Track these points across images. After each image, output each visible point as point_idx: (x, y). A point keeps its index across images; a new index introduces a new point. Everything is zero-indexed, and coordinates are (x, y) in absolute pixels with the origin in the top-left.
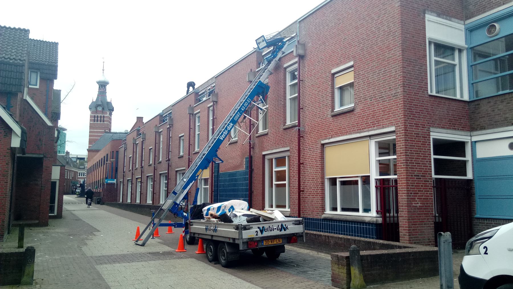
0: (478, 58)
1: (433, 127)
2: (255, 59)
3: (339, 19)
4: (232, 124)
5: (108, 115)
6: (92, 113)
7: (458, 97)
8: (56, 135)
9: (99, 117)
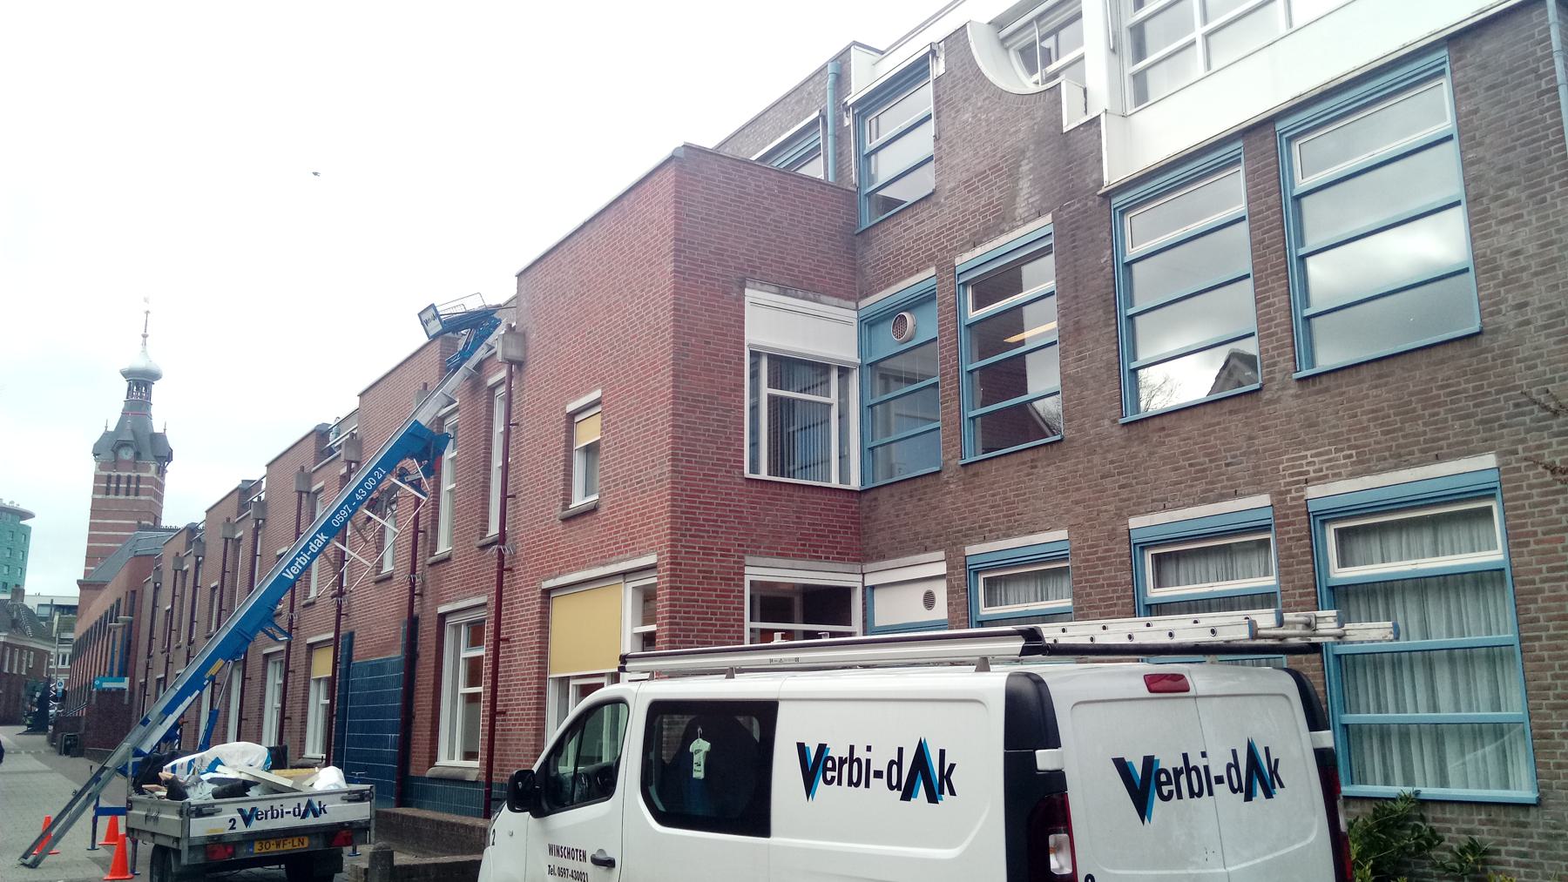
0: (893, 383)
1: (753, 554)
2: (437, 357)
3: (582, 284)
4: (323, 538)
5: (152, 473)
6: (102, 467)
7: (835, 482)
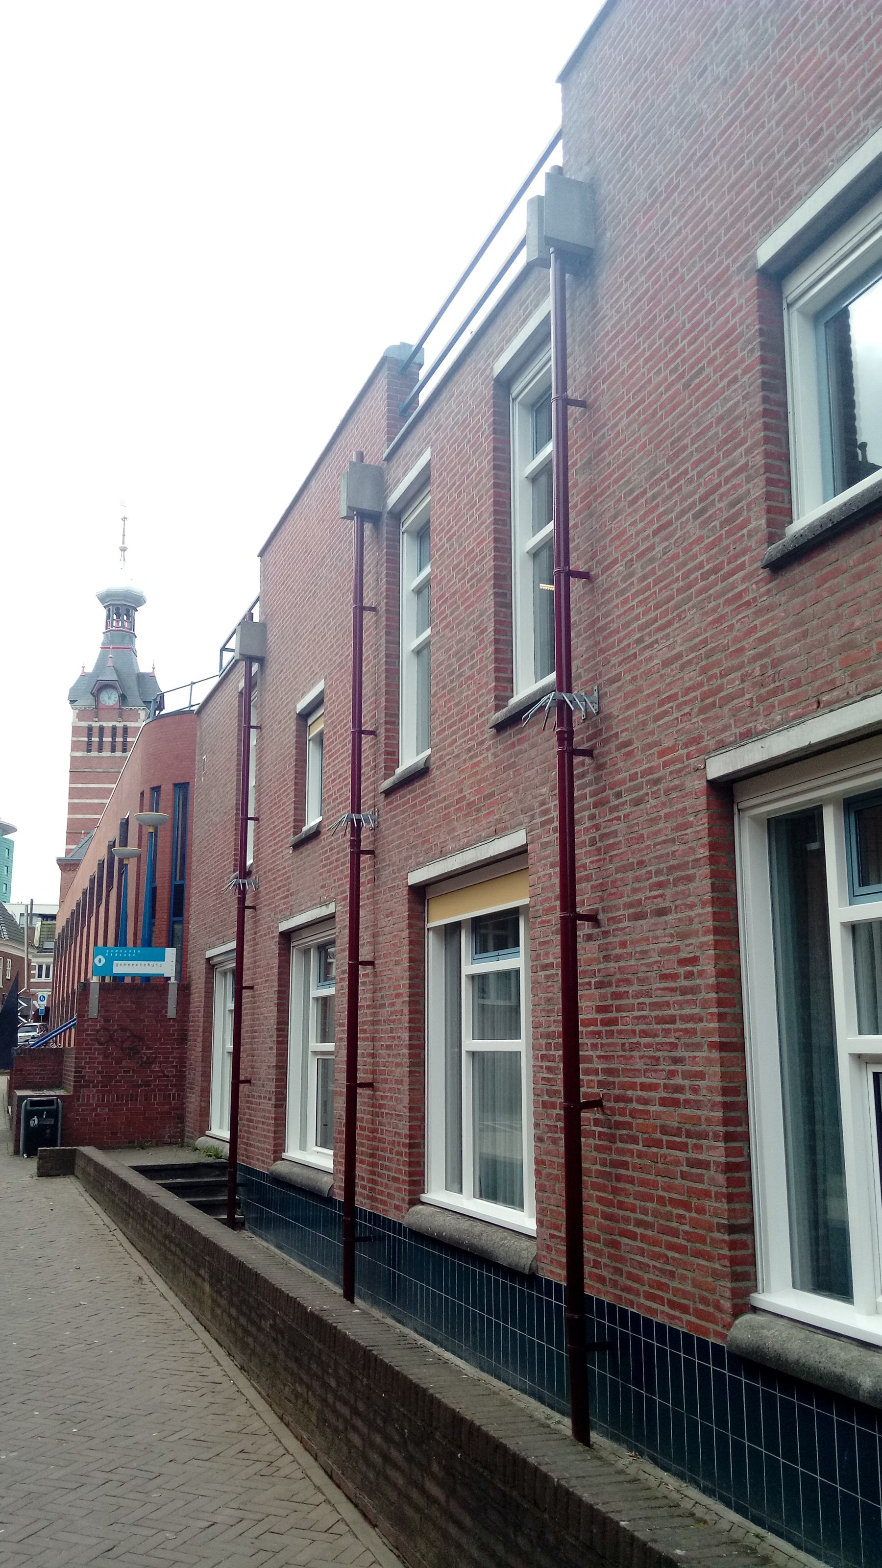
6: (80, 716)
8: (172, 1011)
9: (108, 732)
